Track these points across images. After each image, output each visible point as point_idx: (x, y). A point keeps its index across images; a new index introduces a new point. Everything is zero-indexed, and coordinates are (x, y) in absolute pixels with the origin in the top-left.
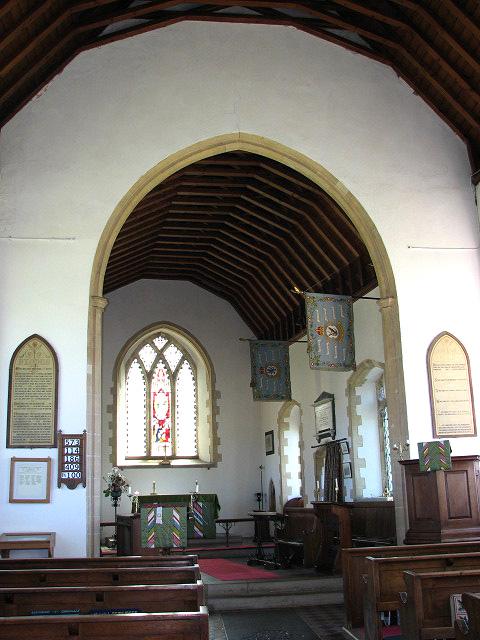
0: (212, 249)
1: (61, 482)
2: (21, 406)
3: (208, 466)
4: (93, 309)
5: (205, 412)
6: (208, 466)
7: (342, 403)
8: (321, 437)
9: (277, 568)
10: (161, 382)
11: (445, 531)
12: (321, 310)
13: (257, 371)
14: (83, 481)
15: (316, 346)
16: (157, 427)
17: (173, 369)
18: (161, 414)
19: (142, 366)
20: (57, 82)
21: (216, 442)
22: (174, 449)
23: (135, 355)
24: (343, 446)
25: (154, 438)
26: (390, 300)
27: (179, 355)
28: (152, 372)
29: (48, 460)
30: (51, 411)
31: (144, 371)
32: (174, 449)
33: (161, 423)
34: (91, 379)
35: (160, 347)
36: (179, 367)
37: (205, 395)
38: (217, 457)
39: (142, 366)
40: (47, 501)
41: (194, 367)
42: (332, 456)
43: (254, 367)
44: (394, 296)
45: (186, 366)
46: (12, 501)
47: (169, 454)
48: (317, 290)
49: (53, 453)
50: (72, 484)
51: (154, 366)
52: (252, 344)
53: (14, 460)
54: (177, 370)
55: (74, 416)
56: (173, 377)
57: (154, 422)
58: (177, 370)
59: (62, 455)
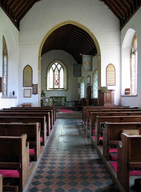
0: (69, 39)
1: (33, 93)
2: (25, 79)
3: (66, 90)
4: (39, 59)
5: (66, 79)
6: (66, 90)
7: (92, 77)
8: (88, 85)
9: (77, 111)
10: (56, 72)
11: (105, 104)
12: (86, 59)
13: (75, 70)
14: (37, 93)
15: (84, 66)
16: (56, 82)
17: (59, 69)
18: (56, 79)
19: (52, 69)
20: (31, 10)
21: (68, 85)
22: (59, 87)
23: (51, 67)
24: (91, 86)
25: (55, 84)
26: (99, 57)
27: (61, 66)
28: (55, 70)
29: (31, 89)
30: (31, 80)
31: (53, 70)
32: (59, 87)
33: (56, 81)
34: (39, 73)
35: (56, 65)
36: (60, 69)
37: (66, 75)
38: (68, 88)
39: (52, 69)
40: (31, 97)
41: (63, 69)
42: (89, 90)
43: (74, 70)
44: (100, 56)
45: (62, 69)
46: (24, 97)
47: (58, 88)
48: (85, 54)
49: (31, 88)
50: (35, 94)
51: (55, 69)
52: (74, 65)
53: (24, 89)
54: (60, 70)
55: (36, 80)
56: (59, 71)
57: (55, 81)
58: (60, 70)
59: (33, 88)
